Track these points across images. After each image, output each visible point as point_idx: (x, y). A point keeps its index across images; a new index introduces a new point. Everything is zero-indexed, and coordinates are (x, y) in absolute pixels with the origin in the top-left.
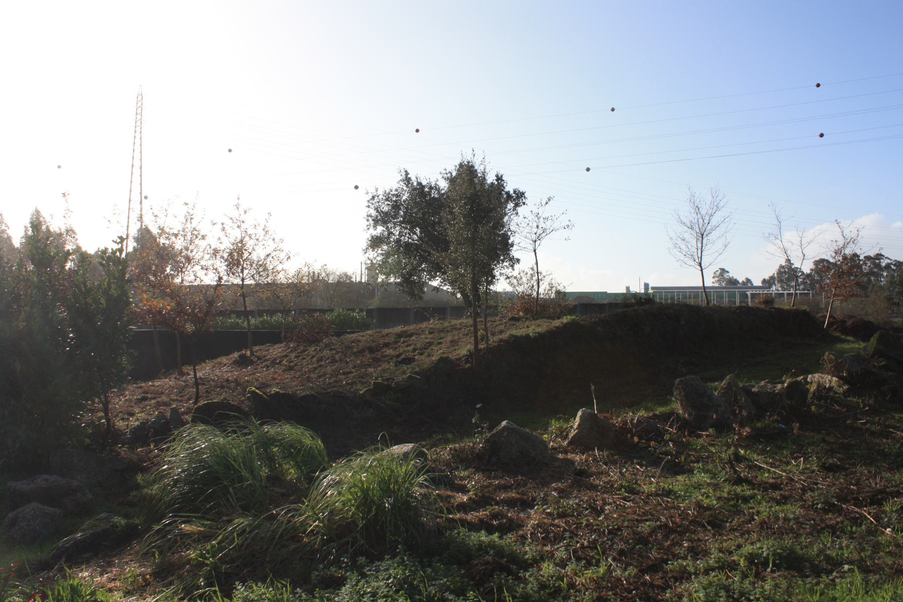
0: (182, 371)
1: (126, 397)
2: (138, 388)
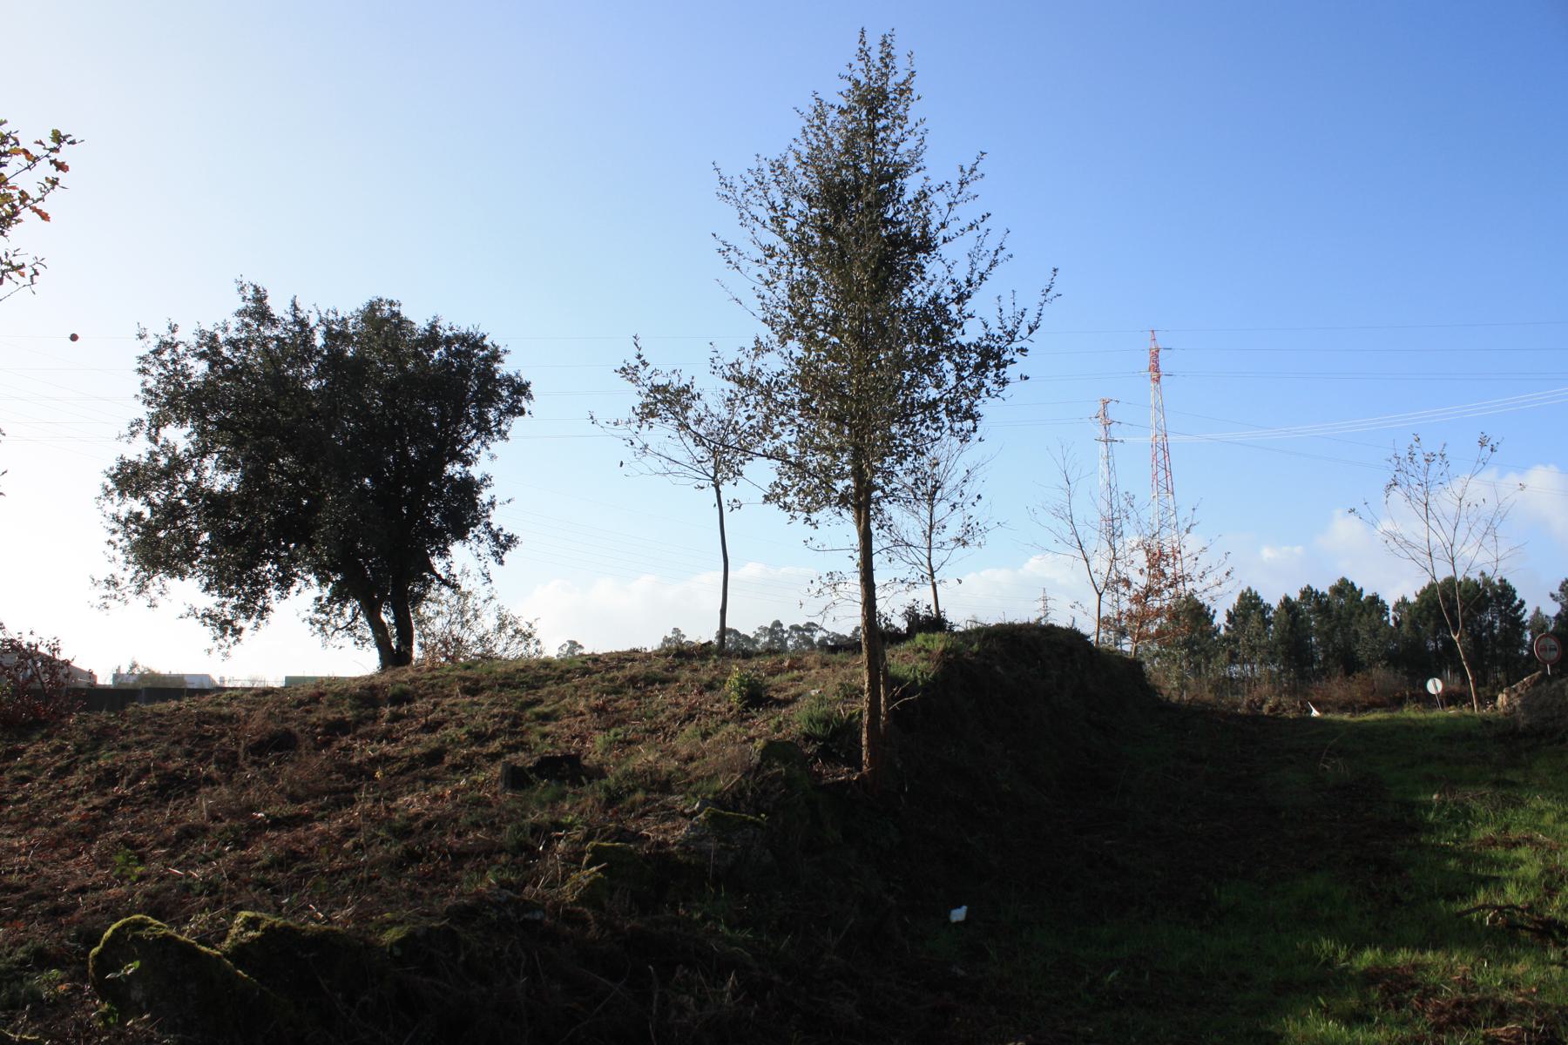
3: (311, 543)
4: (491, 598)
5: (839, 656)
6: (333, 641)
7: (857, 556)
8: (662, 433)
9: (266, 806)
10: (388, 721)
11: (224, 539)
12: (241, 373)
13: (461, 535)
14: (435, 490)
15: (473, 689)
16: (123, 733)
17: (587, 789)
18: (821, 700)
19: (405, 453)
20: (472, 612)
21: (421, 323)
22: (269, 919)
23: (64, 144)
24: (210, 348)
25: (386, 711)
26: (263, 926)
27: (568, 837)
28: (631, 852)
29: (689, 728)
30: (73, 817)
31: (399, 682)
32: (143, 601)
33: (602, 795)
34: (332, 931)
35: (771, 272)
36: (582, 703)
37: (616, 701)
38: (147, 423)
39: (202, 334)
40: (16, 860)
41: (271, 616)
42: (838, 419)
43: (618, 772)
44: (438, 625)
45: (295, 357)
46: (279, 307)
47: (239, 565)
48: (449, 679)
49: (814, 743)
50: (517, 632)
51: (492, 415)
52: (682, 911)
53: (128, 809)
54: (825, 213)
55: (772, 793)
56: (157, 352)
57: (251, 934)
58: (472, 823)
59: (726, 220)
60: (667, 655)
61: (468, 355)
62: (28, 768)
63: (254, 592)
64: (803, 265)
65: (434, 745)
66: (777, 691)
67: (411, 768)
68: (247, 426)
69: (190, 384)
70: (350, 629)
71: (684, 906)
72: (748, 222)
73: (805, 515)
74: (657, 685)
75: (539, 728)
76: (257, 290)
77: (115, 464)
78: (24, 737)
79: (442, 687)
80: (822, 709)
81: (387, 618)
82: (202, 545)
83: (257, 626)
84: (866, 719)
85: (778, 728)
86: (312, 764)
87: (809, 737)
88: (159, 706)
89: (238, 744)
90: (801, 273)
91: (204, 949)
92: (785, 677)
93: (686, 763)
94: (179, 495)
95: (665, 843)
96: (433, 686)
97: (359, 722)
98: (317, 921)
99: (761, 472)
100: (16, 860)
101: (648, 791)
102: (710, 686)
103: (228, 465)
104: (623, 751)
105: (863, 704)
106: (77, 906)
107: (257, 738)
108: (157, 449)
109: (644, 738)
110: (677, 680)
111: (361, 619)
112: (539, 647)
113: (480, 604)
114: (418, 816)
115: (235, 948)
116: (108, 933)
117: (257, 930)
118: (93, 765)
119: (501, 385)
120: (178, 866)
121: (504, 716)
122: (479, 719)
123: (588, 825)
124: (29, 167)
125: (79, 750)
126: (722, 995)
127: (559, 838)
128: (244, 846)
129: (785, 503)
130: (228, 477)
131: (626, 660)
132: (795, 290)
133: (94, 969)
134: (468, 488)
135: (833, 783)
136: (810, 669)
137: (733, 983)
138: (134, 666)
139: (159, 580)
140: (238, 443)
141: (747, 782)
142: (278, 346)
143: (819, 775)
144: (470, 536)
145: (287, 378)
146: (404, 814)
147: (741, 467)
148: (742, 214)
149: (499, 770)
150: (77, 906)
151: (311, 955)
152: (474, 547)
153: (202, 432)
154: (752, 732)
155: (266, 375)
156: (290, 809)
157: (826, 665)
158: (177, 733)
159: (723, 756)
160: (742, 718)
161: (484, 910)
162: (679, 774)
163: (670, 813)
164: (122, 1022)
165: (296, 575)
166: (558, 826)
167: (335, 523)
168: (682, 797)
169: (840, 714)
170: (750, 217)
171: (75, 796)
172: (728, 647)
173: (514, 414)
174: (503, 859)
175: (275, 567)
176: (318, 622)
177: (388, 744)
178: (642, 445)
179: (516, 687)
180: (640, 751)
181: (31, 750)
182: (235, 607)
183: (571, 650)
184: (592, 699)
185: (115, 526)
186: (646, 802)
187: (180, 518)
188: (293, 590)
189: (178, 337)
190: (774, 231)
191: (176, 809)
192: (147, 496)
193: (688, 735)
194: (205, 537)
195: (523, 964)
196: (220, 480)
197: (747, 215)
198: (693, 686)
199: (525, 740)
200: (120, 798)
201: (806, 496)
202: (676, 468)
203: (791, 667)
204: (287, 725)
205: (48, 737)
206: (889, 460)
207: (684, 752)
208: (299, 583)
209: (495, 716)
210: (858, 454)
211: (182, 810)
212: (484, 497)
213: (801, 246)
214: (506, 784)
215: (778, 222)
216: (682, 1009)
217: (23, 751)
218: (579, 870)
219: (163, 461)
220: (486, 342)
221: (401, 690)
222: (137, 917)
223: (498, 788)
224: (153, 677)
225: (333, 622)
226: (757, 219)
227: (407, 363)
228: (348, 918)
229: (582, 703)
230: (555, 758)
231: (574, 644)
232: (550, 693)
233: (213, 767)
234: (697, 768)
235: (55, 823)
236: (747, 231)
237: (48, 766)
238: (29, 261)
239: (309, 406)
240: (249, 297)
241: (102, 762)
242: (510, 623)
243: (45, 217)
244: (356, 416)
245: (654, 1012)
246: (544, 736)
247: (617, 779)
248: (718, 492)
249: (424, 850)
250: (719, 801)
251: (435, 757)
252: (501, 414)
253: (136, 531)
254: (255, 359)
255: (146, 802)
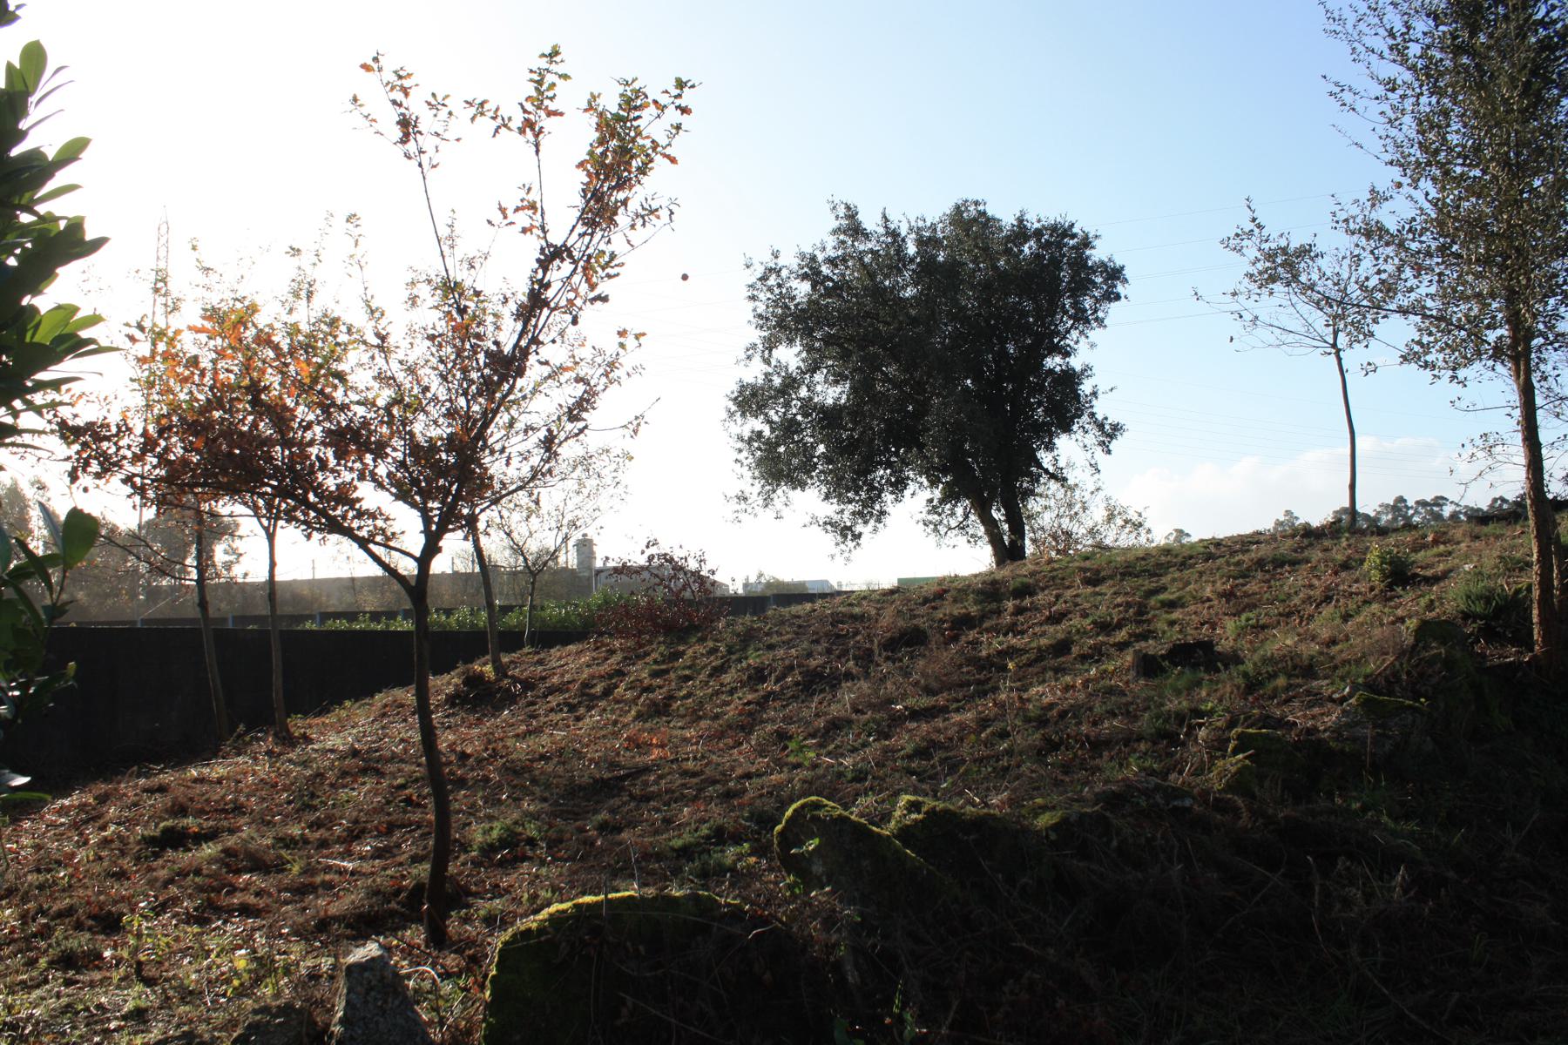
0: (288, 731)
1: (104, 828)
2: (150, 791)
3: (921, 447)
4: (1098, 489)
5: (1490, 528)
6: (947, 540)
7: (1517, 413)
8: (1279, 304)
9: (904, 697)
10: (1012, 614)
11: (839, 450)
12: (841, 289)
13: (1067, 429)
14: (1037, 384)
15: (1094, 580)
16: (767, 634)
17: (1224, 675)
18: (1478, 574)
19: (1004, 350)
20: (1079, 505)
21: (1008, 219)
22: (929, 803)
23: (686, 90)
24: (811, 269)
25: (1010, 605)
26: (924, 809)
27: (1210, 724)
28: (1279, 739)
29: (1327, 611)
30: (731, 712)
31: (1019, 576)
32: (770, 513)
33: (1240, 681)
34: (989, 815)
35: (1393, 107)
36: (1208, 589)
37: (1243, 585)
38: (761, 346)
39: (803, 256)
40: (689, 749)
41: (887, 520)
42: (1486, 261)
43: (1256, 657)
44: (1047, 519)
45: (890, 267)
46: (870, 222)
47: (854, 472)
48: (1068, 571)
49: (1474, 622)
50: (1126, 522)
51: (1088, 303)
52: (1338, 800)
53: (778, 704)
54: (1456, 29)
55: (1430, 676)
56: (763, 279)
57: (914, 816)
58: (1108, 712)
59: (1337, 60)
60: (1293, 536)
61: (1060, 245)
62: (689, 667)
63: (870, 498)
64: (1432, 94)
65: (1061, 636)
66: (1422, 568)
67: (1037, 660)
68: (851, 339)
69: (796, 306)
70: (963, 528)
71: (1340, 796)
72: (1361, 57)
73: (1450, 373)
74: (1287, 567)
75: (1165, 616)
76: (848, 208)
77: (736, 388)
78: (683, 640)
79: (1063, 579)
80: (1481, 585)
81: (997, 514)
82: (818, 457)
83: (875, 530)
84: (1536, 593)
85: (1430, 606)
86: (941, 659)
87: (1466, 616)
88: (795, 609)
89: (872, 642)
90: (1430, 104)
91: (874, 828)
92: (1430, 553)
93: (1328, 646)
94: (794, 411)
95: (1314, 729)
96: (1053, 578)
97: (984, 616)
98: (974, 805)
99: (1397, 331)
100: (689, 749)
101: (1289, 676)
102: (1345, 566)
103: (838, 379)
104: (1257, 637)
105: (1533, 577)
106: (745, 790)
107: (889, 635)
108: (770, 370)
109: (1279, 623)
110: (1308, 561)
111: (972, 517)
112: (1150, 536)
113: (1087, 496)
114: (1051, 706)
115: (900, 829)
116: (789, 813)
117: (919, 813)
118: (744, 664)
119: (1094, 272)
120: (829, 754)
121: (1128, 605)
122: (1103, 608)
123: (1229, 712)
124: (659, 116)
125: (730, 652)
126: (1391, 890)
127: (1200, 725)
128: (887, 737)
129: (1426, 362)
130: (839, 389)
131: (1251, 543)
132: (1425, 124)
133: (779, 844)
134: (1070, 379)
135: (1499, 666)
136: (1458, 543)
137: (1403, 877)
138: (761, 575)
139: (783, 490)
140: (845, 356)
141: (1401, 664)
142: (873, 259)
143: (1483, 656)
144: (1075, 427)
145: (886, 288)
146: (1037, 704)
147: (1374, 327)
148: (1354, 49)
149: (1129, 658)
150: (745, 790)
151: (972, 837)
152: (1080, 438)
153: (809, 349)
154: (1399, 612)
155: (865, 288)
156: (925, 702)
157: (1476, 537)
158: (815, 633)
159: (1370, 638)
160: (1386, 597)
161: (1133, 797)
162: (1322, 658)
163: (1317, 699)
164: (807, 893)
165: (908, 478)
166: (1198, 713)
167: (944, 424)
168: (1327, 681)
169: (1503, 590)
170: (1363, 49)
171: (732, 692)
172: (1349, 524)
173: (1110, 300)
174: (1143, 747)
175: (888, 471)
176: (931, 522)
177: (1015, 636)
178: (1251, 318)
179: (1137, 576)
180: (1275, 636)
181: (690, 652)
182: (853, 513)
183: (1178, 539)
184: (1218, 584)
185: (740, 445)
186: (1289, 687)
187: (796, 432)
188: (907, 493)
189: (781, 262)
190: (1394, 61)
191: (820, 703)
192: (766, 415)
193: (1324, 623)
194: (821, 448)
195: (1176, 851)
196: (831, 393)
197: (1360, 48)
198: (1327, 566)
199: (1151, 628)
200: (770, 693)
201: (1453, 352)
202: (1290, 338)
203: (1436, 542)
204: (915, 622)
205: (702, 640)
206: (1552, 301)
207: (1325, 634)
208: (912, 486)
209: (1119, 605)
210: (1512, 297)
211: (825, 704)
212: (1086, 387)
213: (1429, 73)
214: (1138, 672)
215: (1399, 51)
216: (1347, 903)
217: (683, 653)
218: (1224, 757)
219: (777, 381)
220: (1075, 230)
221: (1022, 583)
222: (814, 798)
223: (1130, 677)
224: (779, 584)
225: (945, 522)
226: (1373, 51)
227: (999, 260)
228: (1002, 802)
229: (1208, 589)
230: (1187, 645)
231: (1180, 532)
232: (1174, 580)
233: (851, 663)
234: (1342, 651)
235: (716, 717)
236: (1361, 67)
237: (706, 665)
238: (665, 203)
239: (907, 314)
240: (842, 215)
241: (751, 661)
242: (1120, 513)
243: (673, 160)
244: (953, 318)
245: (1317, 904)
246: (1172, 623)
247: (1255, 664)
248: (1339, 360)
249: (1061, 738)
250: (1371, 685)
251: (1062, 647)
252: (1097, 301)
253: (759, 449)
254: (851, 274)
255: (793, 697)
